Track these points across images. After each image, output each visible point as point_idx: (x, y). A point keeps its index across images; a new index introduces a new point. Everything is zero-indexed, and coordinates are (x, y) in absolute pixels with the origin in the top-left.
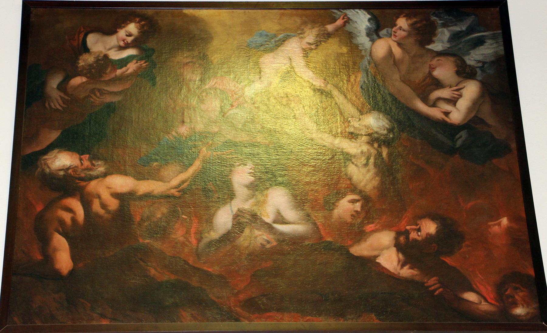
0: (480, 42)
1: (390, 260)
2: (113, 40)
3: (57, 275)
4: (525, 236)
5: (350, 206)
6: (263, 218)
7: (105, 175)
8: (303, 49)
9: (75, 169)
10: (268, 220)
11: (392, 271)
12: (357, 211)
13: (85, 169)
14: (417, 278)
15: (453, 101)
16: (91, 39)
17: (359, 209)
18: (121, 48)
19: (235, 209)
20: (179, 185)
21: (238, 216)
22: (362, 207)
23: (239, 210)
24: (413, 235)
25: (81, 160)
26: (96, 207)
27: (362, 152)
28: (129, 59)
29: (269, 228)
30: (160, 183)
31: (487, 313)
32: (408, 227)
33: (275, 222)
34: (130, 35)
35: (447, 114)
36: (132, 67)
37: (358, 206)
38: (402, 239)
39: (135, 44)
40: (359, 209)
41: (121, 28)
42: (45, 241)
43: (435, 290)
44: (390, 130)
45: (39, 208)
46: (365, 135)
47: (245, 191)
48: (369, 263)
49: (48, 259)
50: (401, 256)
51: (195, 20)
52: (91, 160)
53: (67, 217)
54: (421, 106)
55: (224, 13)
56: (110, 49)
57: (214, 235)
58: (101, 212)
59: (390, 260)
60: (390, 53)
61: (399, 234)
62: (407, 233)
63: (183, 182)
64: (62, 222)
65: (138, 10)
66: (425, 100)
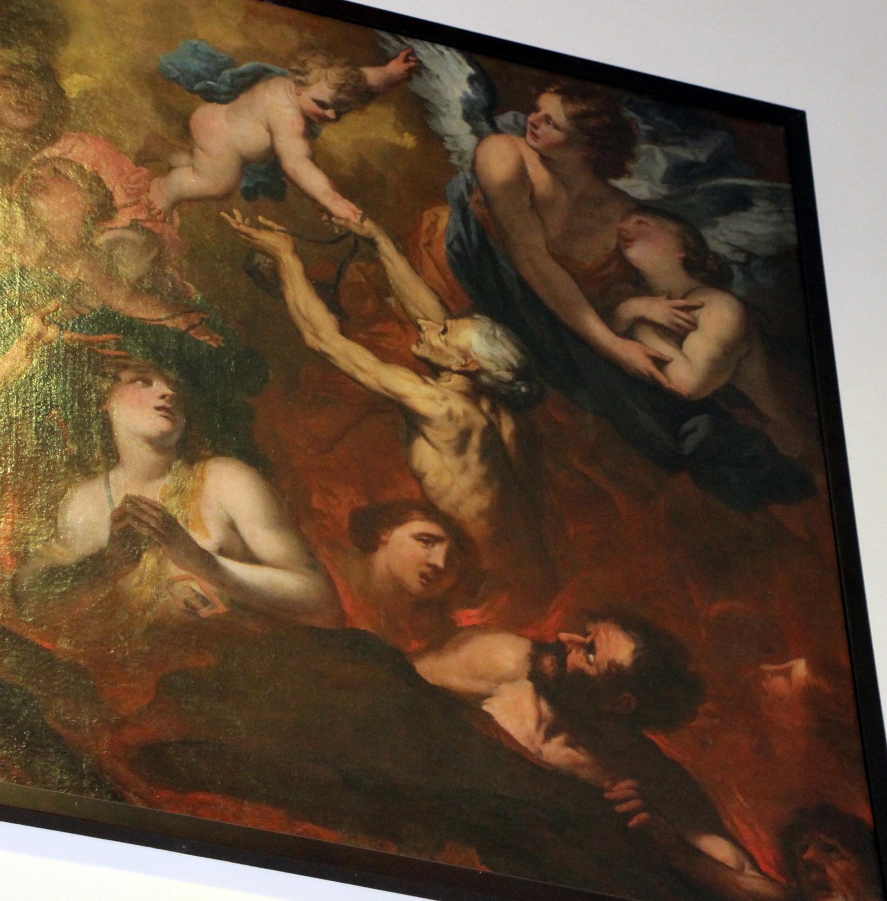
1: (516, 712)
5: (418, 549)
10: (208, 539)
12: (434, 567)
14: (584, 774)
15: (677, 335)
17: (440, 563)
22: (448, 559)
24: (575, 659)
27: (450, 415)
29: (205, 562)
32: (564, 636)
33: (222, 552)
35: (661, 363)
37: (438, 555)
40: (440, 563)
43: (629, 815)
46: (459, 372)
48: (463, 711)
50: (544, 706)
54: (596, 328)
59: (516, 712)
61: (539, 649)
62: (560, 650)
66: (608, 316)
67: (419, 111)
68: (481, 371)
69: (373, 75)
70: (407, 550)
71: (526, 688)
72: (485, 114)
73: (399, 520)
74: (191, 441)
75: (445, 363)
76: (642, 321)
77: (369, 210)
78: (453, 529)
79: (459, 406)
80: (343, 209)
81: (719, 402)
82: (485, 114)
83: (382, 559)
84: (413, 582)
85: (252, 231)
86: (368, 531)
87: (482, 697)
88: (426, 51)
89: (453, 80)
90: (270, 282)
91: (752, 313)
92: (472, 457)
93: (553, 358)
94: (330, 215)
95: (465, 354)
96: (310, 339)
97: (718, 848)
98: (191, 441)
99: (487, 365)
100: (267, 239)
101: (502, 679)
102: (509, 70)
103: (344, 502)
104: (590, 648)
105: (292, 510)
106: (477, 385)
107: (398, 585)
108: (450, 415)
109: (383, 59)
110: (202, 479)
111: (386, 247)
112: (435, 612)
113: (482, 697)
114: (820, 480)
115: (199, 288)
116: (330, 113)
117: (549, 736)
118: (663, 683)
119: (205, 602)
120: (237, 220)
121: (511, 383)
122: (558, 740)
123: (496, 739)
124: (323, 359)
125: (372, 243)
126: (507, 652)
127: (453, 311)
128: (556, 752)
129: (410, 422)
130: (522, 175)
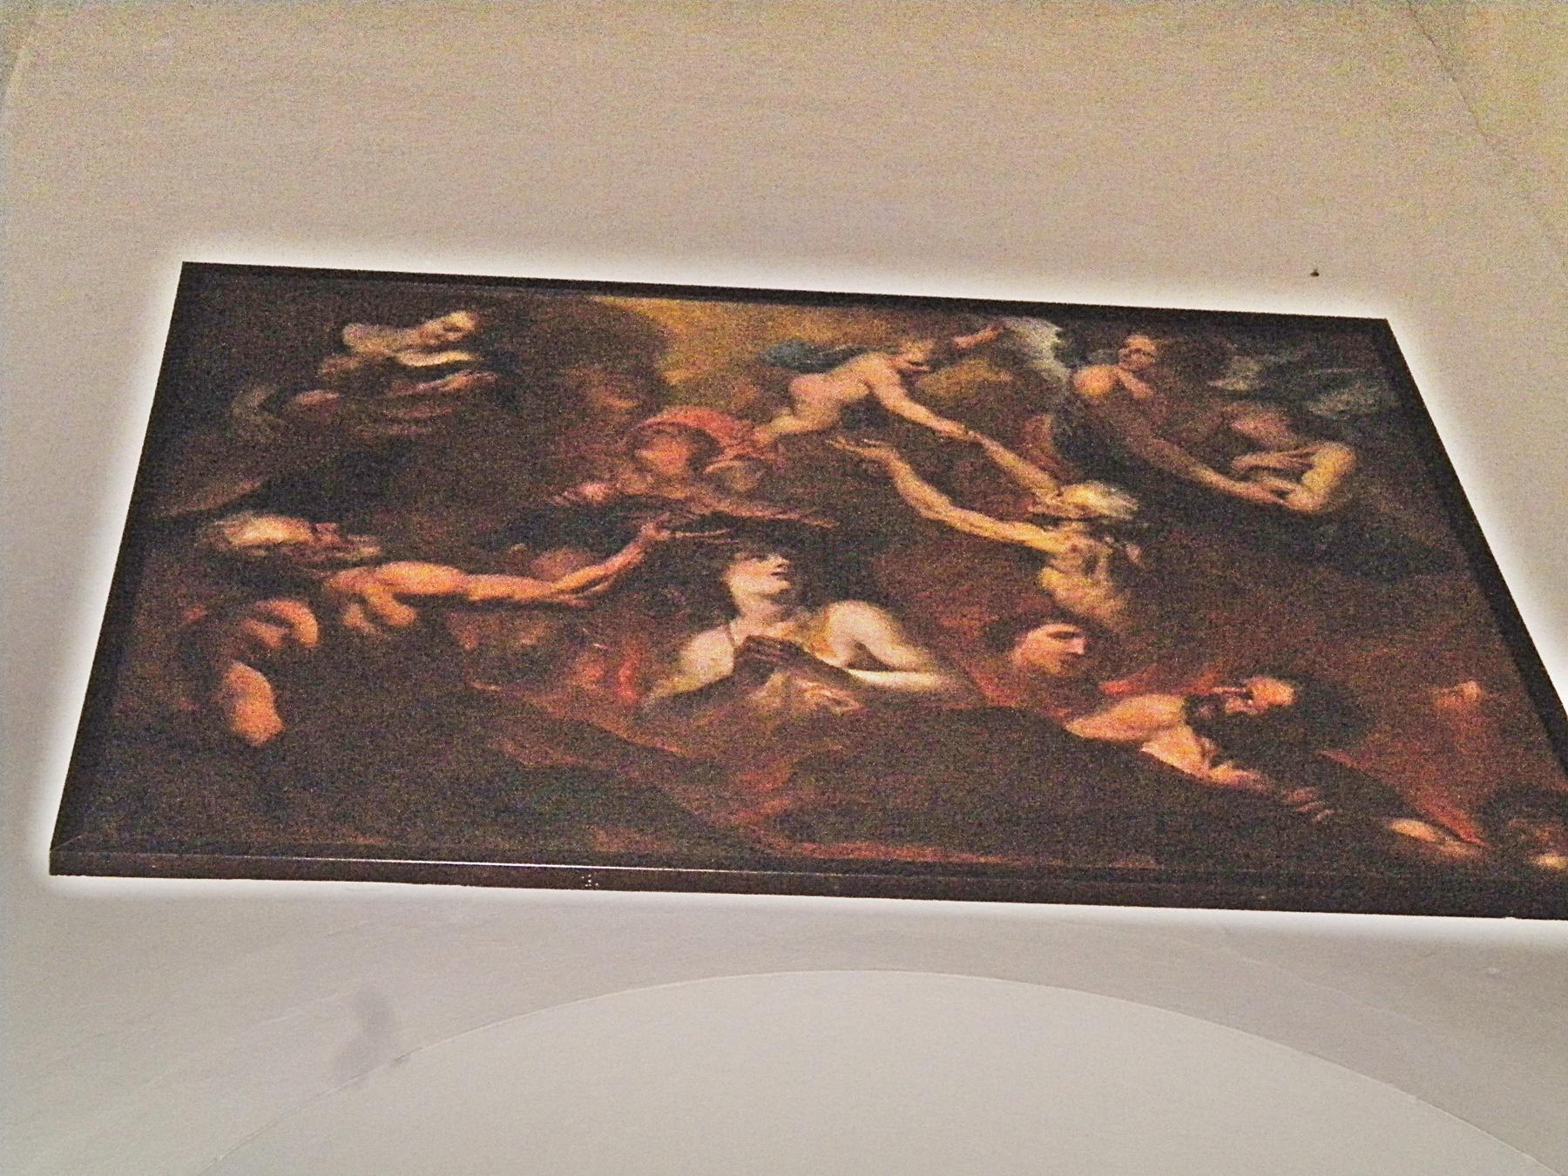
0: (1339, 383)
1: (1179, 751)
2: (412, 336)
3: (240, 747)
4: (939, 316)
5: (1057, 645)
6: (818, 656)
7: (377, 562)
8: (900, 372)
9: (299, 547)
10: (837, 658)
11: (1188, 771)
12: (1075, 655)
13: (326, 549)
14: (1384, 819)
15: (1296, 475)
16: (351, 333)
17: (1080, 651)
18: (429, 350)
19: (739, 640)
20: (583, 588)
21: (749, 649)
22: (1087, 647)
23: (749, 638)
24: (1233, 705)
25: (314, 530)
26: (354, 616)
27: (1074, 549)
28: (454, 367)
29: (838, 676)
30: (529, 581)
31: (1453, 864)
32: (1219, 690)
33: (851, 666)
34: (455, 329)
35: (1282, 494)
36: (457, 381)
37: (1078, 646)
38: (1204, 711)
39: (468, 342)
40: (1080, 651)
41: (432, 316)
42: (206, 679)
43: (1316, 811)
44: (1137, 515)
45: (195, 612)
46: (1078, 520)
47: (769, 608)
48: (1122, 756)
49: (214, 708)
50: (1207, 743)
51: (646, 322)
52: (342, 532)
53: (270, 634)
54: (1210, 477)
55: (697, 308)
56: (398, 351)
57: (682, 684)
58: (367, 627)
59: (1179, 751)
60: (1118, 385)
61: (1193, 703)
62: (1217, 702)
63: (594, 583)
64: (258, 645)
65: (487, 292)
66: (1223, 470)
67: (1015, 358)
68: (1102, 516)
69: (962, 341)
70: (1042, 644)
71: (1185, 734)
72: (1076, 354)
73: (1037, 624)
74: (810, 592)
75: (1063, 515)
76: (1256, 468)
77: (972, 424)
78: (1087, 624)
79: (1083, 543)
80: (946, 426)
81: (1345, 513)
82: (1076, 354)
83: (1017, 656)
84: (1054, 668)
85: (859, 450)
86: (1002, 637)
87: (1138, 743)
88: (1011, 322)
89: (1043, 338)
90: (885, 478)
91: (1366, 453)
92: (1101, 575)
93: (1167, 504)
94: (934, 432)
95: (1083, 508)
96: (924, 513)
97: (1550, 860)
98: (810, 592)
99: (1106, 512)
100: (873, 453)
101: (1161, 727)
102: (1089, 328)
103: (971, 619)
104: (1249, 696)
105: (917, 627)
106: (1094, 524)
107: (1040, 672)
108: (1074, 549)
109: (972, 330)
110: (827, 618)
111: (995, 449)
112: (1082, 686)
113: (1138, 743)
114: (1461, 554)
115: (515, 543)
116: (925, 368)
117: (1214, 764)
118: (1326, 711)
119: (839, 703)
120: (841, 442)
121: (1133, 522)
122: (1222, 767)
123: (1167, 776)
124: (940, 525)
125: (977, 445)
126: (1165, 707)
127: (1063, 479)
128: (1224, 773)
129: (1038, 558)
130: (1118, 385)
